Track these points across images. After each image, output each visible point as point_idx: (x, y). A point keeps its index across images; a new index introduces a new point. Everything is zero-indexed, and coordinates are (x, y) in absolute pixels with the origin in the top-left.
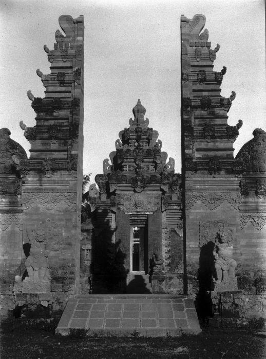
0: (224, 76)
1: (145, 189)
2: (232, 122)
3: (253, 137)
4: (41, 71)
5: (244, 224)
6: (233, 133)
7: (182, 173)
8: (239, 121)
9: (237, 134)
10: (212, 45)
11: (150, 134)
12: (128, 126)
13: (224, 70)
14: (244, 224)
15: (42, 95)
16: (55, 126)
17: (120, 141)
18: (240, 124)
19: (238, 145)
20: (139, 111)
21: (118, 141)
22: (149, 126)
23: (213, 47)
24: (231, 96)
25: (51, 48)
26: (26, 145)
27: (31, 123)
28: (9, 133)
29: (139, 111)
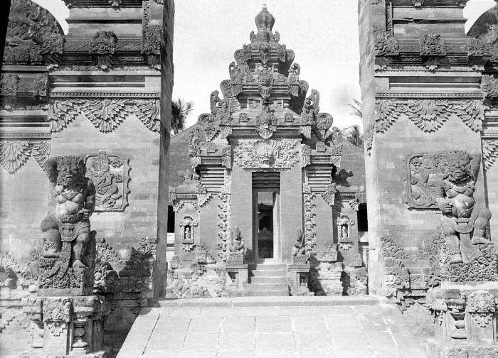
22: (281, 43)
29: (266, 21)
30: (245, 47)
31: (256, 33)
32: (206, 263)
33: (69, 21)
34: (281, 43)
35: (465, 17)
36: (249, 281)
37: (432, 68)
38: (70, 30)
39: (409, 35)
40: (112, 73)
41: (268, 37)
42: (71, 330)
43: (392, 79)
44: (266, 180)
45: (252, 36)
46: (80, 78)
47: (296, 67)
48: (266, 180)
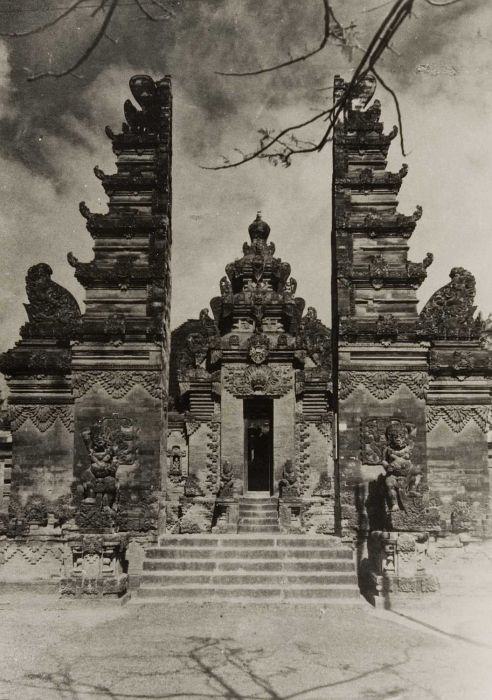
0: (428, 269)
1: (332, 130)
2: (415, 256)
3: (449, 280)
4: (100, 168)
5: (433, 422)
6: (416, 277)
7: (333, 326)
8: (403, 165)
9: (424, 276)
10: (385, 126)
11: (279, 275)
12: (240, 255)
13: (429, 260)
14: (433, 422)
15: (104, 210)
16: (128, 256)
17: (228, 280)
18: (429, 260)
19: (423, 294)
20: (259, 231)
21: (224, 280)
22: (276, 256)
23: (386, 132)
24: (415, 214)
25: (118, 131)
26: (79, 292)
27: (86, 256)
28: (50, 272)
29: (259, 231)
30: (237, 262)
31: (249, 244)
32: (194, 496)
33: (86, 303)
34: (276, 256)
35: (418, 298)
36: (70, 256)
37: (387, 344)
38: (87, 310)
39: (369, 314)
40: (120, 348)
41: (258, 251)
42: (253, 452)
43: (353, 353)
44: (259, 409)
45: (246, 248)
46: (96, 352)
47: (294, 283)
48: (259, 409)
